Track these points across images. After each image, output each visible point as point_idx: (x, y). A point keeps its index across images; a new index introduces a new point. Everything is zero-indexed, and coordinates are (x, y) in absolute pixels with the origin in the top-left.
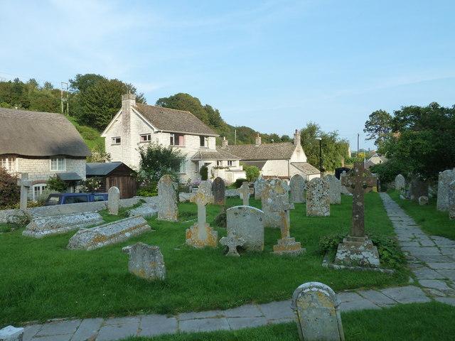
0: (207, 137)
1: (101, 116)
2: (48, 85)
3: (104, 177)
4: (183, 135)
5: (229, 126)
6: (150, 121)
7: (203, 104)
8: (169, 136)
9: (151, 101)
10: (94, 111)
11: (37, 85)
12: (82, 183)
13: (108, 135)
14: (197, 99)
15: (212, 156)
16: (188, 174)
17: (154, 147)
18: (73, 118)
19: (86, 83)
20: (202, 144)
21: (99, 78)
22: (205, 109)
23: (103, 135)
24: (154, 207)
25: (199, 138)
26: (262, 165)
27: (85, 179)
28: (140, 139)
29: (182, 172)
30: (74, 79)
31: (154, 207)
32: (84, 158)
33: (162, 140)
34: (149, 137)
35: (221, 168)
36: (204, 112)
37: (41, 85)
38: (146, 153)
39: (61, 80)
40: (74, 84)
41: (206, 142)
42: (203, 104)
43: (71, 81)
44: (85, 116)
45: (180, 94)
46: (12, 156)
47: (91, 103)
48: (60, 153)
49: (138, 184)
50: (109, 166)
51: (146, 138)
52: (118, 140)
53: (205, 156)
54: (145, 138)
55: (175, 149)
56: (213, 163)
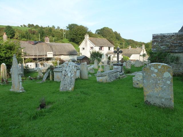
0: (111, 47)
1: (77, 39)
2: (58, 28)
3: (81, 60)
4: (103, 47)
5: (124, 39)
6: (93, 43)
7: (114, 31)
8: (99, 47)
9: (94, 32)
10: (74, 37)
11: (55, 27)
12: (76, 61)
13: (81, 47)
14: (111, 29)
15: (112, 53)
16: (104, 59)
17: (94, 51)
18: (68, 39)
19: (72, 27)
20: (109, 49)
21: (76, 25)
22: (114, 33)
23: (79, 47)
24: (94, 66)
25: (108, 48)
26: (131, 56)
27: (77, 60)
28: (90, 48)
29: (102, 58)
30: (68, 26)
31: (94, 66)
32: (76, 55)
33: (97, 49)
34: (93, 48)
35: (115, 57)
36: (114, 34)
37: (56, 28)
38: (92, 52)
39: (63, 25)
40: (67, 28)
41: (110, 49)
42: (114, 31)
43: (67, 27)
44: (71, 39)
45: (105, 28)
46: (61, 55)
47: (73, 34)
48: (71, 54)
49: (90, 62)
50: (81, 57)
51: (92, 48)
52: (84, 49)
53: (110, 53)
54: (92, 48)
55: (100, 51)
56: (113, 56)
